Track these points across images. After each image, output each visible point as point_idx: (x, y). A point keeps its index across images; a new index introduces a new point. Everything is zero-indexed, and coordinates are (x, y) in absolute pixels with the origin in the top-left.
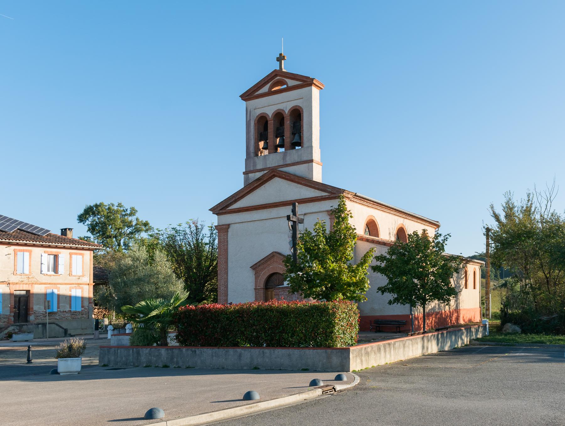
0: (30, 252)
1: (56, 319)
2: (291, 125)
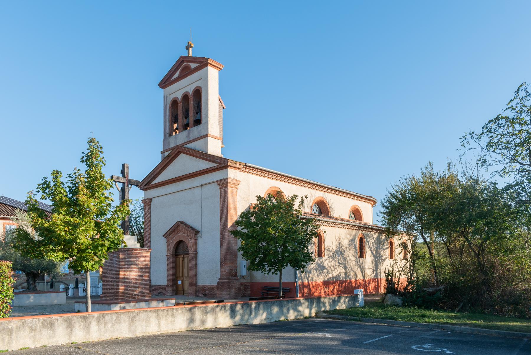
2: (196, 105)
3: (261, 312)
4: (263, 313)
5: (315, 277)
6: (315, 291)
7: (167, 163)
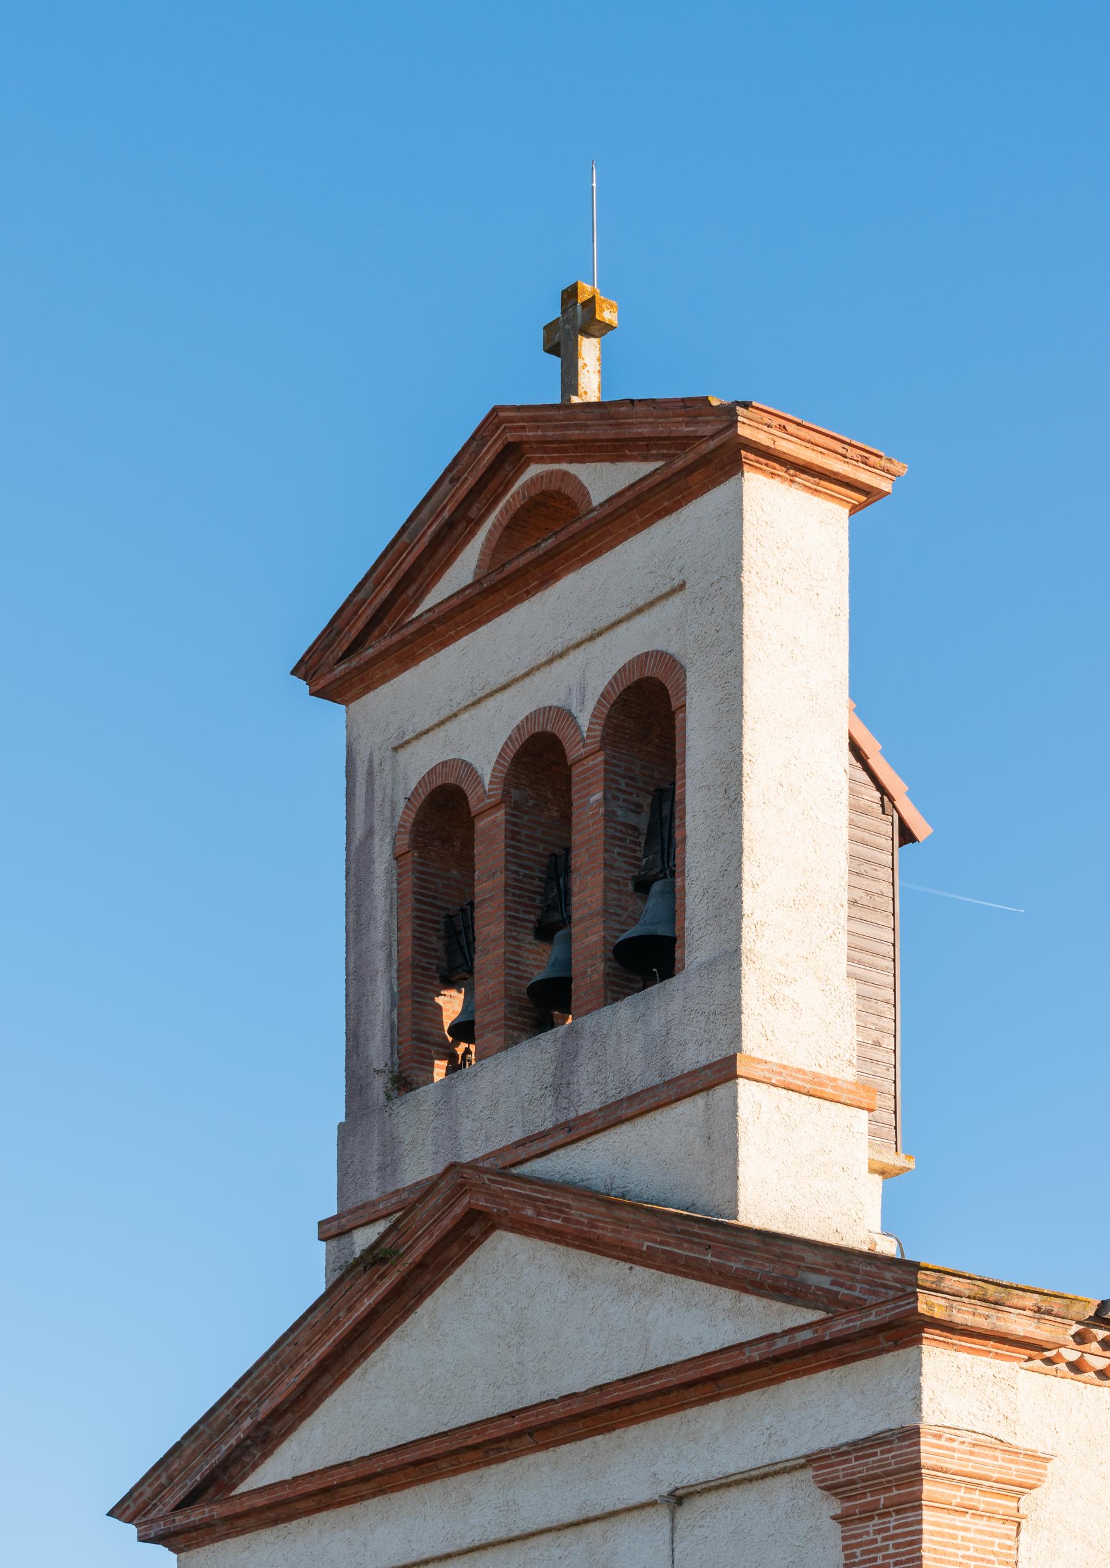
2: (632, 819)
7: (372, 1315)
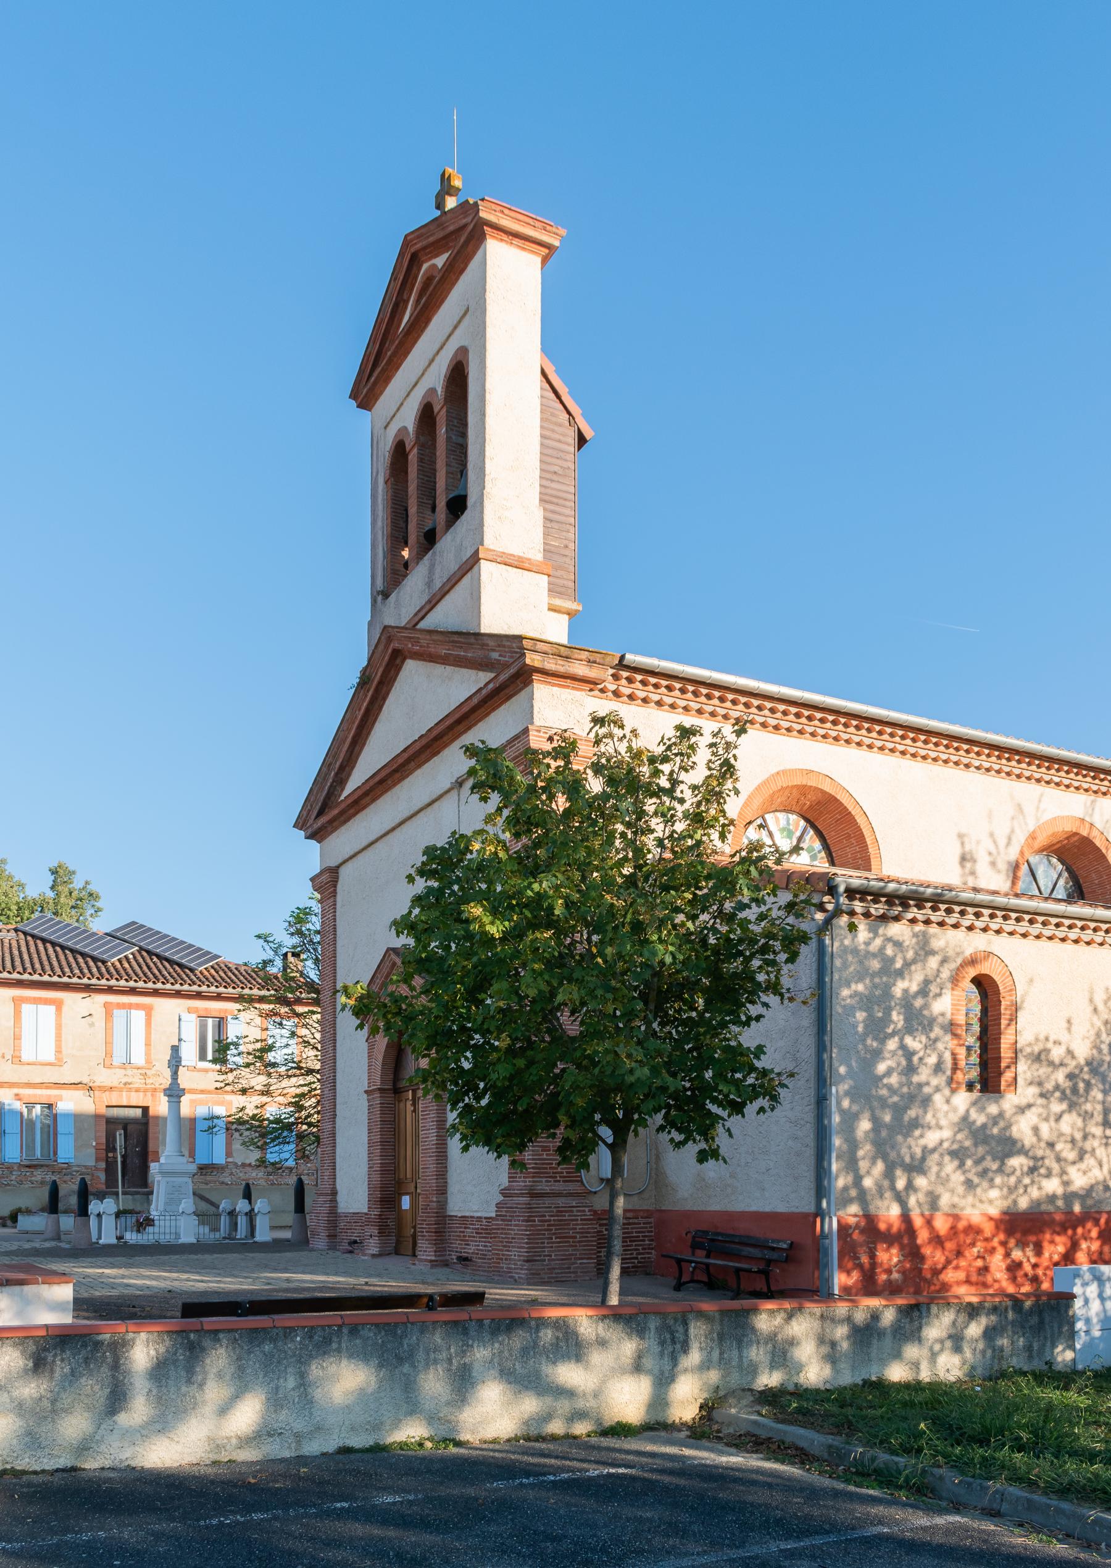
0: (148, 1010)
1: (223, 1183)
3: (214, 1392)
4: (236, 1397)
5: (952, 1191)
6: (948, 1262)
7: (368, 711)
